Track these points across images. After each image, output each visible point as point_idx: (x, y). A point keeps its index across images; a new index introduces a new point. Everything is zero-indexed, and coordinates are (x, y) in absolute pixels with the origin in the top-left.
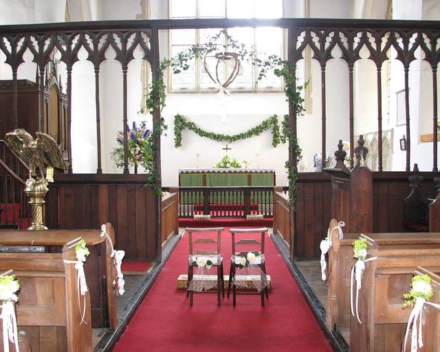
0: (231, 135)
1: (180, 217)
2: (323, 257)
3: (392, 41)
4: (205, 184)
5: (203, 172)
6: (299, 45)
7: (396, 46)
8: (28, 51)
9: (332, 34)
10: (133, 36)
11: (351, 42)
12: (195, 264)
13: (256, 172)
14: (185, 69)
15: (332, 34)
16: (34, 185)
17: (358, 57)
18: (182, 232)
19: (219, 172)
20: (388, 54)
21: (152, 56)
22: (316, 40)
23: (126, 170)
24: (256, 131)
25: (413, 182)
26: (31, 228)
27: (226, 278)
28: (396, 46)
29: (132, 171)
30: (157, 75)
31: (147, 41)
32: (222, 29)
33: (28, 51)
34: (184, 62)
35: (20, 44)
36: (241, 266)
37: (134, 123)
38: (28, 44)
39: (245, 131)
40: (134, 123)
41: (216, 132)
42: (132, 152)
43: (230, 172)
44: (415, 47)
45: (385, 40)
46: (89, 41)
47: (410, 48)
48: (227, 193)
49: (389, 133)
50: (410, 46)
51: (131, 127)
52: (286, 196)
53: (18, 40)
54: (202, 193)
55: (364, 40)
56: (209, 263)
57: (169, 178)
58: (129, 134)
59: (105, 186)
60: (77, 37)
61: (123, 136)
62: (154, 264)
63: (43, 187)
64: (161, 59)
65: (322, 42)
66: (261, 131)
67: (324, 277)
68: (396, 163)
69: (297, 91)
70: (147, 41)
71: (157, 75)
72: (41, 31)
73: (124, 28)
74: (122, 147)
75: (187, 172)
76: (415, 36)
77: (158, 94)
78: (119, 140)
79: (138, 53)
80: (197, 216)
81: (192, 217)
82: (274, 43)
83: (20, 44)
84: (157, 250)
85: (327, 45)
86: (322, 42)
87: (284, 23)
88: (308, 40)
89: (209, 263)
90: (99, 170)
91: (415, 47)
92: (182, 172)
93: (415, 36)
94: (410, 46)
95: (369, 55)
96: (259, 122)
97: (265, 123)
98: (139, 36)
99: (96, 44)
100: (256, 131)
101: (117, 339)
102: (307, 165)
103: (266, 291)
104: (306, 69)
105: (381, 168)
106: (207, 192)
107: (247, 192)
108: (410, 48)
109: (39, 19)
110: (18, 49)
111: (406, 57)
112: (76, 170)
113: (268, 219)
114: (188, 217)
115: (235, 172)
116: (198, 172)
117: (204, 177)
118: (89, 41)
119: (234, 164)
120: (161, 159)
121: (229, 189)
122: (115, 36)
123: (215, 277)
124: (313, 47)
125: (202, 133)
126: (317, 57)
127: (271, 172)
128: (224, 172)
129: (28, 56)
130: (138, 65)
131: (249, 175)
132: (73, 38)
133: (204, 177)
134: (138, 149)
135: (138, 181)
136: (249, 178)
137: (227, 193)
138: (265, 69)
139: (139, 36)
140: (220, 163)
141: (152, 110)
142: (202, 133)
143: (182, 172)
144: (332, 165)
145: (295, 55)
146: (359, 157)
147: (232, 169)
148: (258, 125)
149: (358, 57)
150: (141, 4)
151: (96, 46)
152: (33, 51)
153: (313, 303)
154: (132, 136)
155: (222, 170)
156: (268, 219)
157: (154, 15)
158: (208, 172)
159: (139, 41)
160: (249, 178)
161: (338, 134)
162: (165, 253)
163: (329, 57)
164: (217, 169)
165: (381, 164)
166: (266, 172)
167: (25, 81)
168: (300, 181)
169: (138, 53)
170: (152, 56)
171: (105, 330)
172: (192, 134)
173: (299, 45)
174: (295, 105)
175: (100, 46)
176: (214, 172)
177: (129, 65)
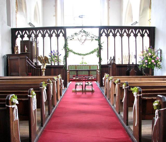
0: (84, 54)
1: (70, 78)
2: (103, 81)
4: (76, 69)
5: (76, 65)
6: (101, 32)
8: (146, 33)
9: (110, 30)
10: (53, 30)
12: (77, 85)
13: (92, 65)
14: (73, 39)
15: (110, 30)
17: (116, 35)
19: (80, 65)
21: (65, 35)
23: (51, 64)
24: (92, 52)
25: (128, 66)
27: (84, 89)
30: (66, 40)
31: (63, 31)
32: (82, 29)
33: (146, 33)
34: (73, 37)
36: (87, 85)
37: (54, 50)
39: (89, 52)
40: (54, 50)
41: (79, 53)
42: (54, 59)
43: (84, 65)
47: (129, 33)
48: (83, 71)
49: (132, 53)
51: (53, 52)
52: (99, 71)
53: (30, 31)
54: (76, 71)
56: (80, 84)
58: (52, 54)
60: (46, 30)
61: (50, 54)
64: (67, 37)
66: (94, 52)
67: (104, 85)
69: (101, 44)
70: (63, 31)
71: (66, 40)
73: (57, 28)
74: (50, 58)
75: (71, 65)
77: (66, 45)
78: (49, 56)
79: (61, 34)
80: (74, 78)
81: (73, 79)
82: (96, 32)
85: (108, 33)
86: (107, 32)
88: (104, 31)
89: (80, 84)
92: (69, 66)
93: (124, 30)
95: (119, 35)
96: (93, 50)
97: (95, 50)
98: (104, 30)
100: (92, 52)
102: (104, 62)
103: (92, 91)
104: (104, 38)
105: (122, 63)
106: (77, 71)
108: (129, 33)
111: (142, 36)
113: (95, 79)
114: (72, 78)
115: (85, 65)
116: (74, 65)
117: (76, 67)
119: (85, 63)
120: (105, 64)
121: (82, 70)
123: (82, 89)
125: (74, 53)
127: (97, 65)
128: (82, 65)
130: (61, 38)
131: (90, 66)
132: (44, 31)
133: (76, 67)
134: (55, 58)
135: (62, 67)
136: (90, 67)
137: (83, 71)
138: (93, 39)
140: (63, 61)
141: (65, 49)
142: (74, 53)
143: (69, 66)
145: (101, 35)
146: (113, 61)
147: (85, 64)
148: (93, 51)
149: (116, 35)
150: (55, 12)
154: (54, 54)
155: (81, 65)
156: (95, 79)
158: (77, 65)
160: (90, 67)
161: (111, 55)
163: (109, 35)
164: (80, 65)
166: (95, 65)
169: (61, 34)
170: (65, 35)
172: (72, 53)
173: (101, 32)
174: (101, 48)
175: (51, 33)
176: (79, 65)
177: (59, 38)
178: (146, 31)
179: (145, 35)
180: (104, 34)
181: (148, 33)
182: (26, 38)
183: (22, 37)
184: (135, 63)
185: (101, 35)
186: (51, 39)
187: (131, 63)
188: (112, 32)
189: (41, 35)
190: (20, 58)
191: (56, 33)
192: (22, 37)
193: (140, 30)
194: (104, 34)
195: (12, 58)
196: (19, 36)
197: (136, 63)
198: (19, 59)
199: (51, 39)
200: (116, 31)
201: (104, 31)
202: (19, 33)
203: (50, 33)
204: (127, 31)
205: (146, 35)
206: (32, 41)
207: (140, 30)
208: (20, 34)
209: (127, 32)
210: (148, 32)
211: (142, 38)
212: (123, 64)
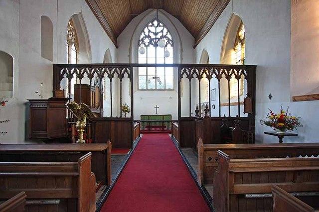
3: (204, 71)
7: (215, 73)
8: (233, 74)
11: (228, 72)
16: (80, 124)
17: (202, 77)
18: (141, 135)
20: (222, 76)
22: (187, 71)
25: (223, 121)
26: (77, 142)
28: (215, 73)
29: (123, 117)
33: (233, 74)
35: (83, 71)
38: (85, 71)
44: (222, 73)
45: (240, 71)
46: (108, 70)
50: (220, 73)
55: (233, 72)
57: (137, 117)
59: (113, 122)
62: (130, 150)
63: (84, 124)
65: (190, 72)
68: (214, 113)
72: (91, 66)
73: (121, 66)
76: (232, 70)
79: (126, 75)
83: (83, 71)
84: (132, 144)
86: (190, 72)
87: (174, 65)
88: (185, 71)
90: (111, 116)
91: (222, 73)
93: (232, 70)
94: (220, 73)
98: (233, 70)
99: (110, 71)
101: (110, 191)
107: (162, 122)
109: (93, 62)
110: (82, 72)
112: (104, 116)
118: (108, 70)
122: (117, 69)
124: (225, 74)
126: (198, 77)
129: (85, 75)
130: (126, 81)
132: (102, 69)
139: (126, 69)
144: (194, 115)
149: (202, 77)
151: (90, 72)
152: (118, 73)
153: (190, 169)
157: (133, 62)
159: (126, 71)
162: (135, 143)
165: (165, 70)
167: (86, 84)
168: (181, 120)
169: (126, 75)
171: (106, 187)
178: (224, 70)
179: (232, 76)
180: (185, 76)
181: (246, 74)
182: (85, 80)
183: (80, 77)
184: (227, 116)
185: (180, 77)
186: (121, 80)
187: (222, 116)
188: (196, 73)
189: (127, 75)
190: (50, 107)
191: (119, 72)
192: (80, 77)
193: (235, 70)
194: (185, 76)
195: (41, 106)
196: (65, 75)
197: (111, 114)
198: (48, 108)
199: (121, 80)
200: (231, 72)
201: (185, 71)
202: (65, 72)
203: (80, 73)
204: (236, 72)
205: (243, 76)
206: (91, 83)
207: (235, 70)
208: (66, 73)
209: (236, 73)
210: (245, 72)
211: (237, 81)
212: (126, 117)
